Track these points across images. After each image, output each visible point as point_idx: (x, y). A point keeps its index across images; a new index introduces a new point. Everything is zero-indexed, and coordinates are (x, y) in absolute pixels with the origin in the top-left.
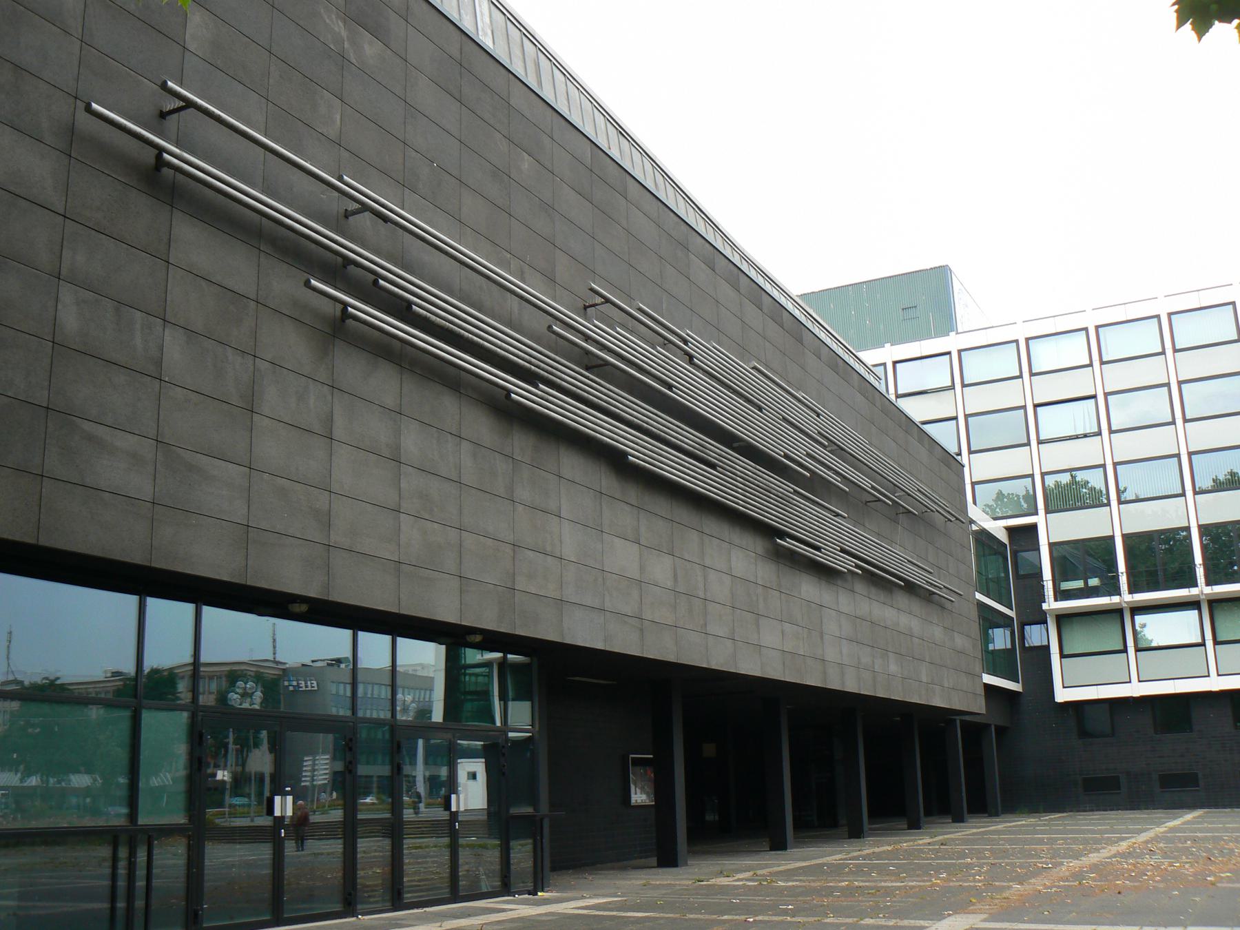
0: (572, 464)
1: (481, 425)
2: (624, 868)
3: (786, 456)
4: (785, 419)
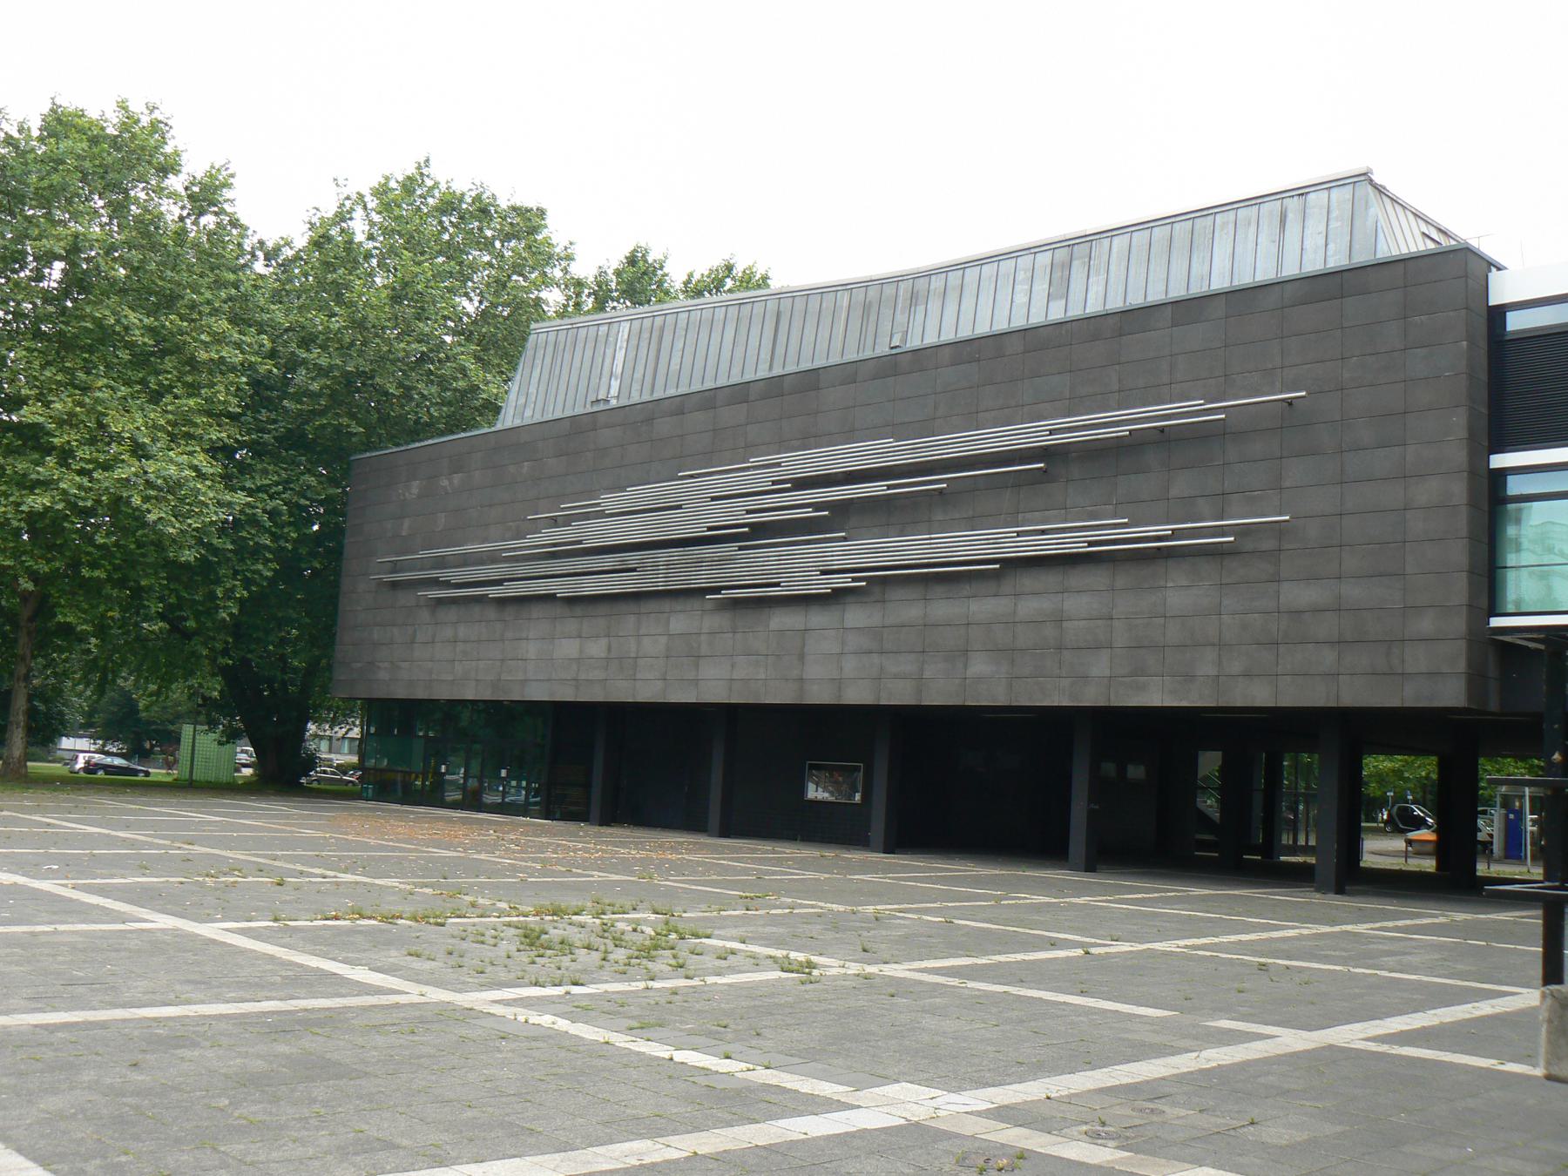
0: (537, 611)
1: (491, 613)
3: (710, 529)
4: (713, 499)
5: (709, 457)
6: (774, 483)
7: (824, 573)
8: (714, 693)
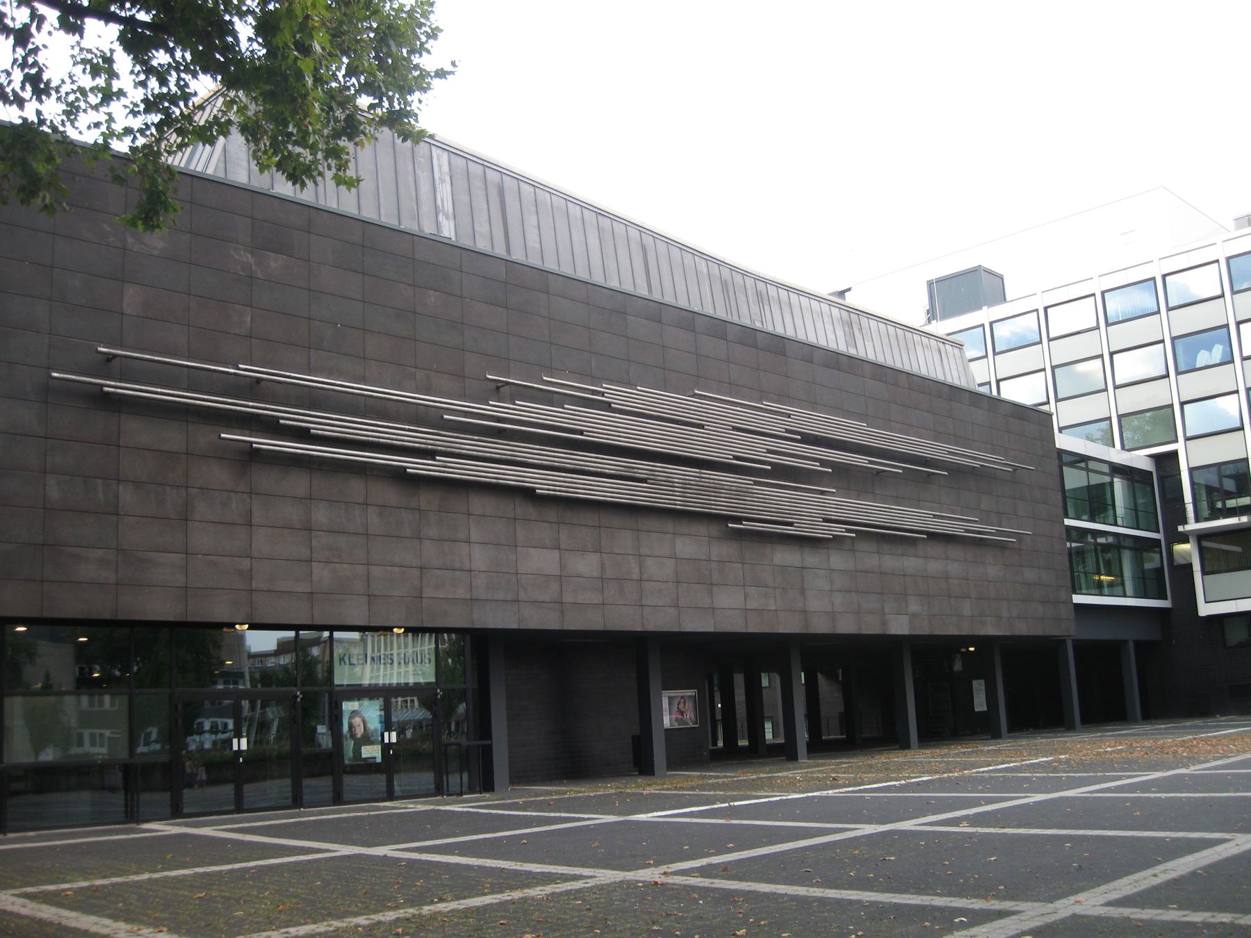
0: (479, 504)
1: (389, 494)
2: (1210, 722)
3: (736, 458)
4: (735, 429)
5: (733, 388)
6: (787, 431)
7: (826, 520)
8: (732, 623)
